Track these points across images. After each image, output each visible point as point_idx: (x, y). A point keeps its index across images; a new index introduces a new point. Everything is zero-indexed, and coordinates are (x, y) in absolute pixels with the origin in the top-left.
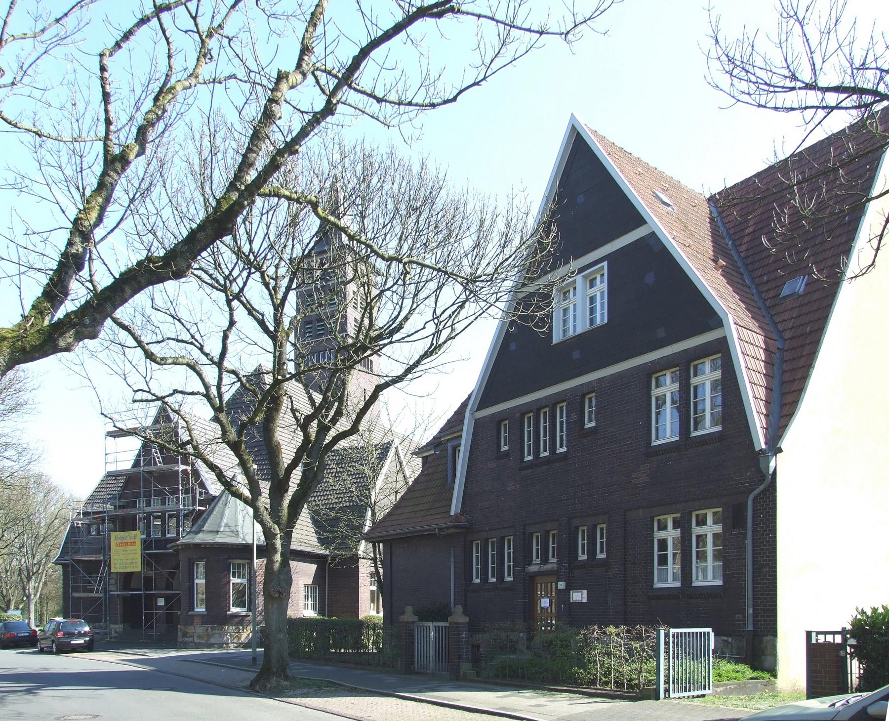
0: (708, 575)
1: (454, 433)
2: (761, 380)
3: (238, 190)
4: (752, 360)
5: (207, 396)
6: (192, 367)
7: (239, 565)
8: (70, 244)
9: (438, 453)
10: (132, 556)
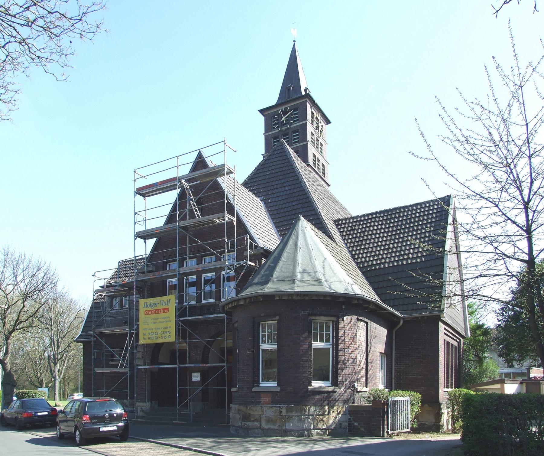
10: (164, 325)
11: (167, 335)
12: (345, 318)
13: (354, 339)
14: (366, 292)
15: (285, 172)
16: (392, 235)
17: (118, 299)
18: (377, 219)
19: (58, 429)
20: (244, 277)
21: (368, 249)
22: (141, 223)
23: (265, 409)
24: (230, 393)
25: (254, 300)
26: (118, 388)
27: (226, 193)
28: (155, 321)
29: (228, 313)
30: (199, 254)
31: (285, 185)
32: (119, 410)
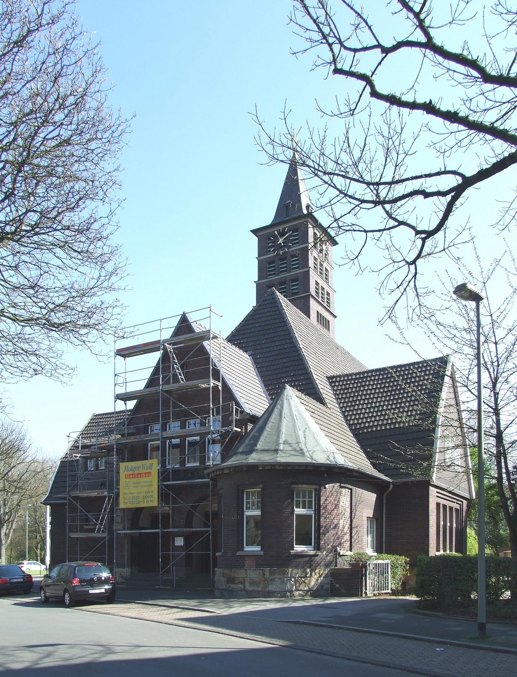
11: (150, 499)
12: (327, 486)
13: (337, 506)
14: (355, 459)
15: (276, 325)
16: (387, 396)
17: (93, 461)
18: (373, 378)
19: (42, 593)
20: (230, 443)
21: (361, 409)
22: (122, 385)
23: (248, 572)
24: (215, 558)
25: (239, 469)
27: (211, 356)
28: (136, 485)
29: (212, 479)
30: (184, 417)
31: (275, 339)
32: (105, 574)
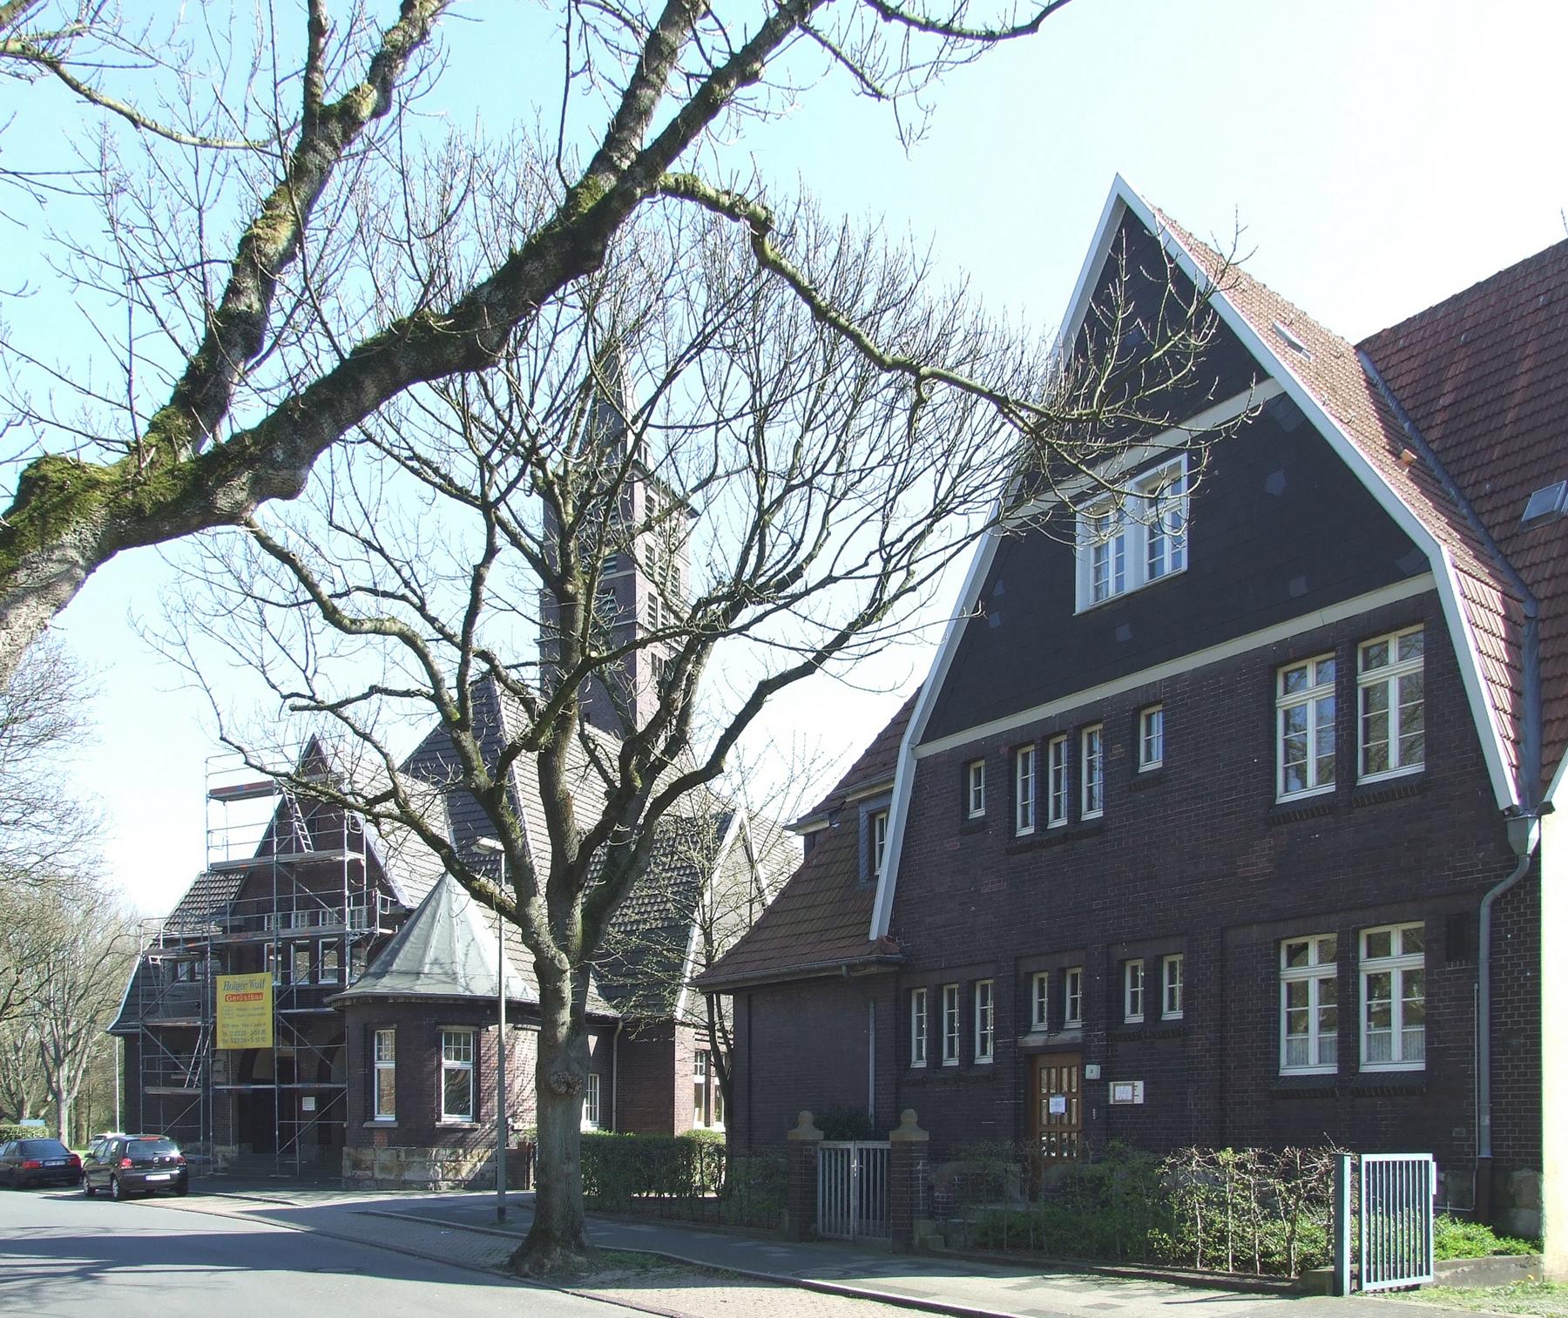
0: (1395, 1052)
1: (873, 786)
2: (1501, 674)
3: (615, 169)
4: (1485, 635)
5: (437, 698)
6: (409, 639)
7: (458, 1036)
8: (233, 290)
9: (840, 825)
10: (255, 1020)
26: (179, 1119)
32: (175, 1153)
